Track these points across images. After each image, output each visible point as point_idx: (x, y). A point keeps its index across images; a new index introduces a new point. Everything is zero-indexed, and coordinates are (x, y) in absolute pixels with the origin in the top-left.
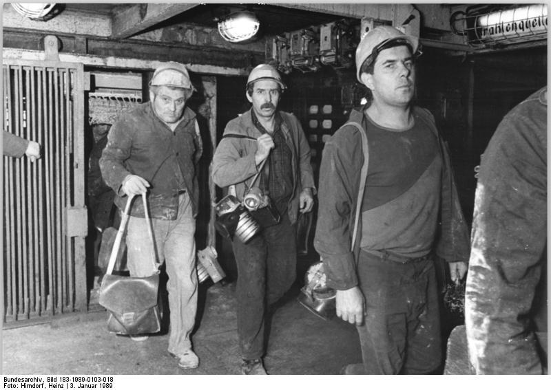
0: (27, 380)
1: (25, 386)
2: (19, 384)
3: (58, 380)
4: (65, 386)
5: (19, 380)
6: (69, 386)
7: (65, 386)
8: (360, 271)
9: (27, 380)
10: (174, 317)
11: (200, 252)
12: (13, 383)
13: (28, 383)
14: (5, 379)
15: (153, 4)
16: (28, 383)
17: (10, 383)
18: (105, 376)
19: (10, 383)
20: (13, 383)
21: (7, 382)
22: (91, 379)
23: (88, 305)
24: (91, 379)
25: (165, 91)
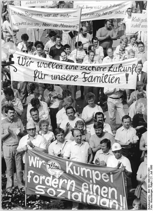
0: (149, 201)
1: (151, 201)
2: (151, 204)
3: (149, 189)
4: (152, 181)
5: (149, 204)
6: (151, 179)
7: (152, 181)
8: (136, 32)
9: (149, 201)
10: (102, 29)
11: (119, 23)
12: (150, 206)
13: (150, 200)
14: (149, 209)
15: (36, 147)
16: (150, 200)
17: (150, 207)
18: (148, 187)
19: (150, 207)
20: (150, 206)
21: (150, 208)
22: (149, 169)
23: (127, 80)
24: (149, 169)
25: (65, 101)
